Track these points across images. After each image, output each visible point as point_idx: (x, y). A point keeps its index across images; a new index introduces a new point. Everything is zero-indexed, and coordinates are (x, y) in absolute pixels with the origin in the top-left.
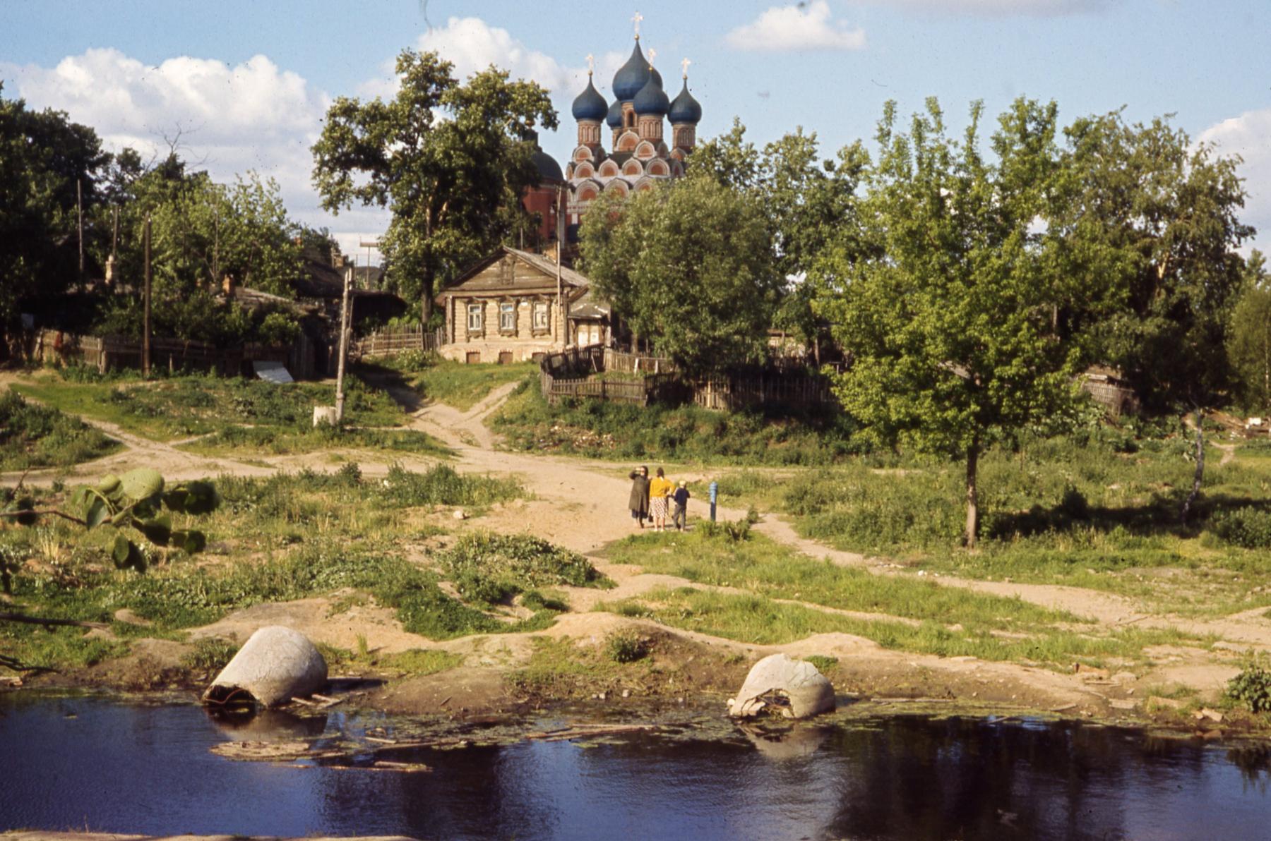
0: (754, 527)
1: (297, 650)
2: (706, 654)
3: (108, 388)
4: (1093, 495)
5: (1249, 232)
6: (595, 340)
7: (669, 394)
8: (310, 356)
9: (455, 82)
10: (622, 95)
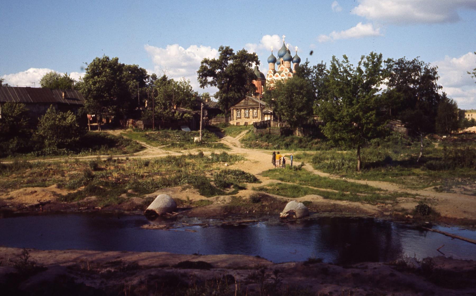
0: (303, 167)
1: (168, 200)
2: (277, 201)
3: (143, 133)
4: (394, 157)
5: (441, 87)
6: (269, 119)
7: (286, 132)
8: (193, 124)
9: (234, 54)
10: (281, 57)
